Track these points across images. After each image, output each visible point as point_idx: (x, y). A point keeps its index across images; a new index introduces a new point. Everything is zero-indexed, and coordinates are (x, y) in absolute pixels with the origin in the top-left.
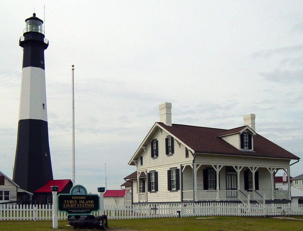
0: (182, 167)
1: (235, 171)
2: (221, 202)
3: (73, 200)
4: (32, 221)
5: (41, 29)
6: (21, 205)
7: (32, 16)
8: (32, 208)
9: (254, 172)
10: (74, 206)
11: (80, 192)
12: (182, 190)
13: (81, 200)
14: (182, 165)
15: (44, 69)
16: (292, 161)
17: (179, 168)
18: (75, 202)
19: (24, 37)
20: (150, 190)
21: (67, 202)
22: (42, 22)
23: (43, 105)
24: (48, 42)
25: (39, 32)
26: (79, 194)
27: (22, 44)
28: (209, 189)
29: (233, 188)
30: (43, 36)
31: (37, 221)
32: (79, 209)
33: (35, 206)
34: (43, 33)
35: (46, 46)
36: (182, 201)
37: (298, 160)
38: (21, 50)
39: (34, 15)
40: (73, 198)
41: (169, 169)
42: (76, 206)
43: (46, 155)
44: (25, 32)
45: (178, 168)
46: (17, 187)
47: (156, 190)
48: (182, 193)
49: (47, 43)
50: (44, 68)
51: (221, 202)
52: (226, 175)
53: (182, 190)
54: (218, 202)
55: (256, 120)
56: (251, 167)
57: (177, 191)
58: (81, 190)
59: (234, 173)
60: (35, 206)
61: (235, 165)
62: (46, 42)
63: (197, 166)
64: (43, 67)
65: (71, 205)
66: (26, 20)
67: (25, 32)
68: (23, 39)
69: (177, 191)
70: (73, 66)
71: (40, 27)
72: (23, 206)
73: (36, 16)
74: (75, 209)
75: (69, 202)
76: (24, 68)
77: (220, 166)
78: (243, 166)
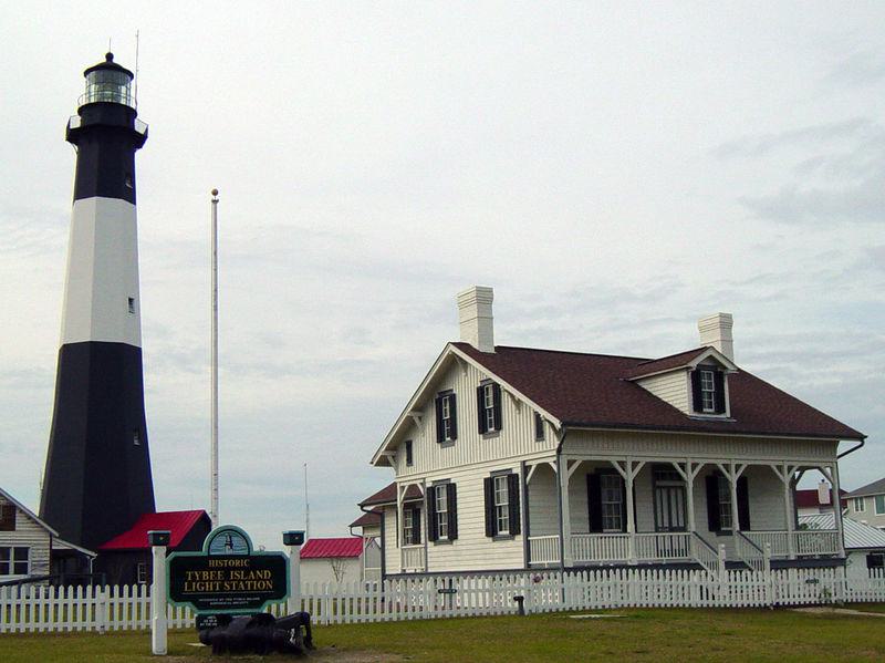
0: (526, 469)
1: (680, 478)
2: (640, 567)
3: (212, 569)
4: (94, 633)
5: (128, 96)
6: (61, 588)
7: (104, 60)
8: (94, 596)
9: (733, 478)
10: (214, 586)
11: (231, 545)
12: (528, 534)
13: (235, 568)
14: (527, 464)
15: (135, 204)
16: (844, 446)
17: (517, 470)
18: (216, 575)
19: (79, 118)
20: (434, 537)
21: (193, 576)
22: (132, 76)
23: (131, 300)
24: (147, 130)
25: (123, 102)
26: (228, 551)
27: (73, 136)
28: (605, 531)
29: (675, 524)
30: (132, 113)
31: (107, 634)
32: (228, 596)
33: (103, 591)
34: (133, 106)
35: (140, 140)
36: (529, 566)
37: (859, 443)
38: (71, 152)
39: (109, 56)
40: (212, 563)
41: (488, 476)
42: (222, 587)
43: (136, 443)
44: (84, 102)
45: (514, 472)
46: (51, 535)
47: (453, 535)
48: (528, 544)
49: (142, 132)
50: (133, 201)
51: (640, 567)
52: (655, 487)
53: (528, 534)
54: (634, 567)
55: (735, 330)
56: (777, 467)
57: (513, 539)
58: (235, 540)
59: (678, 484)
60: (103, 591)
61: (777, 463)
62: (139, 128)
63: (570, 463)
64: (130, 197)
65: (205, 585)
66: (87, 73)
67: (84, 103)
68: (76, 123)
69: (513, 539)
70: (215, 193)
71: (123, 89)
72: (66, 591)
73: (115, 60)
74: (219, 596)
75: (201, 576)
76: (92, 202)
77: (635, 464)
78: (702, 463)
